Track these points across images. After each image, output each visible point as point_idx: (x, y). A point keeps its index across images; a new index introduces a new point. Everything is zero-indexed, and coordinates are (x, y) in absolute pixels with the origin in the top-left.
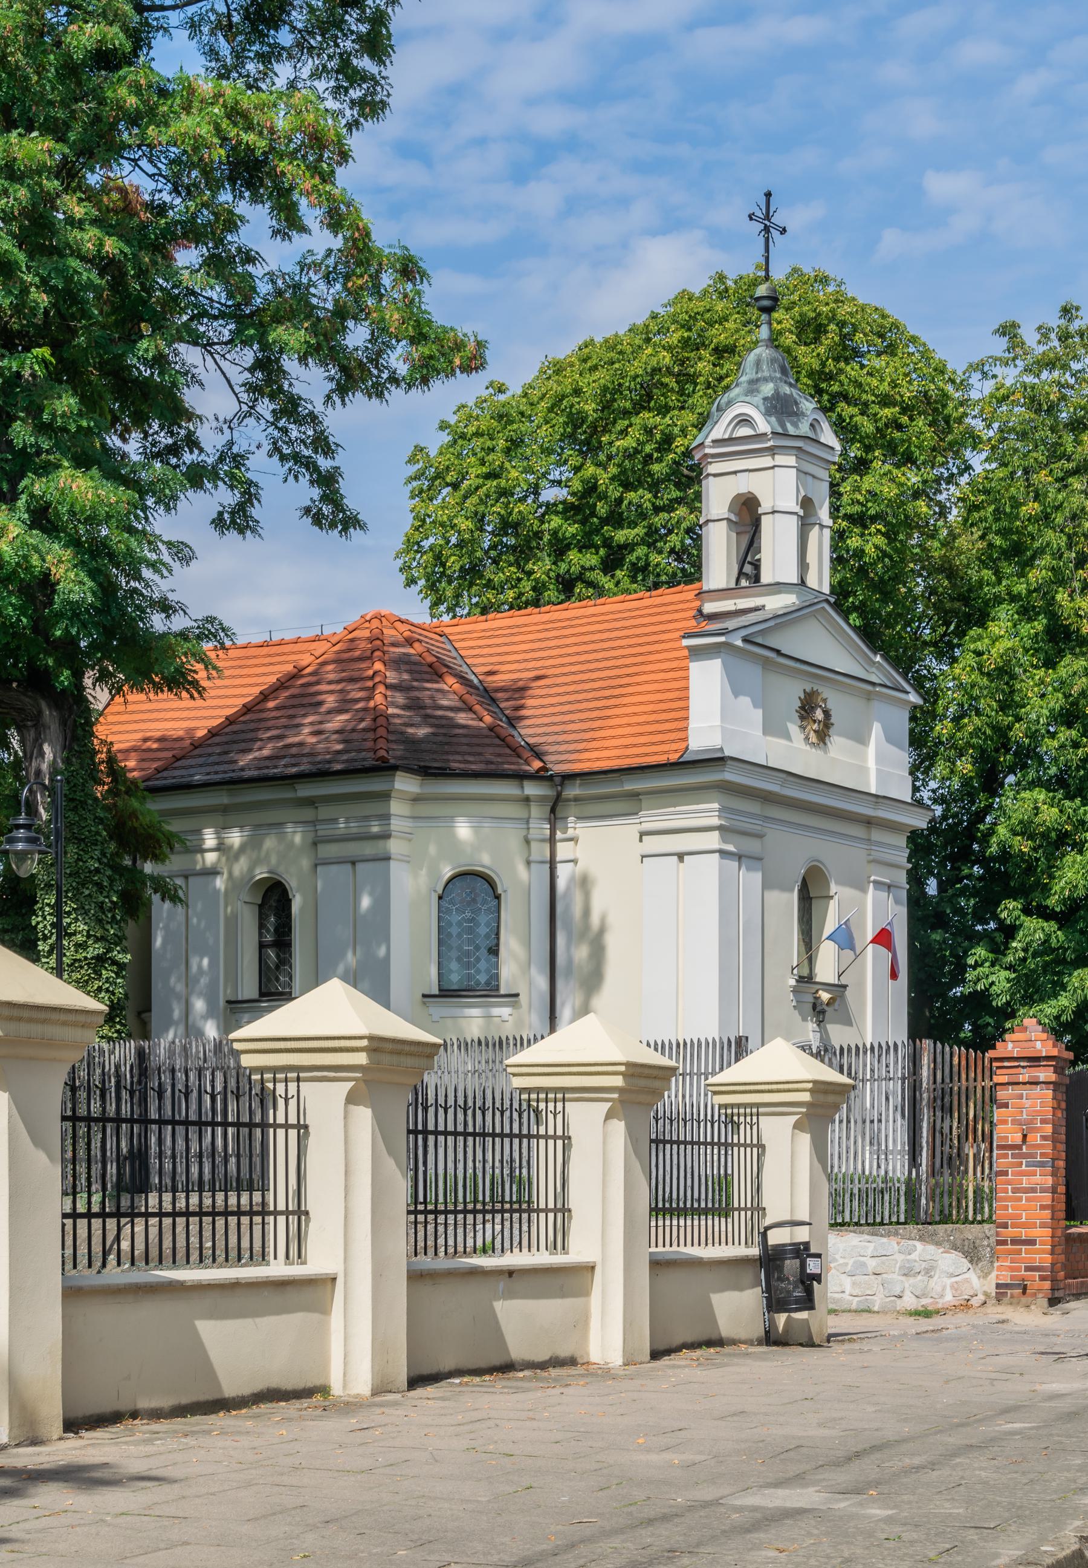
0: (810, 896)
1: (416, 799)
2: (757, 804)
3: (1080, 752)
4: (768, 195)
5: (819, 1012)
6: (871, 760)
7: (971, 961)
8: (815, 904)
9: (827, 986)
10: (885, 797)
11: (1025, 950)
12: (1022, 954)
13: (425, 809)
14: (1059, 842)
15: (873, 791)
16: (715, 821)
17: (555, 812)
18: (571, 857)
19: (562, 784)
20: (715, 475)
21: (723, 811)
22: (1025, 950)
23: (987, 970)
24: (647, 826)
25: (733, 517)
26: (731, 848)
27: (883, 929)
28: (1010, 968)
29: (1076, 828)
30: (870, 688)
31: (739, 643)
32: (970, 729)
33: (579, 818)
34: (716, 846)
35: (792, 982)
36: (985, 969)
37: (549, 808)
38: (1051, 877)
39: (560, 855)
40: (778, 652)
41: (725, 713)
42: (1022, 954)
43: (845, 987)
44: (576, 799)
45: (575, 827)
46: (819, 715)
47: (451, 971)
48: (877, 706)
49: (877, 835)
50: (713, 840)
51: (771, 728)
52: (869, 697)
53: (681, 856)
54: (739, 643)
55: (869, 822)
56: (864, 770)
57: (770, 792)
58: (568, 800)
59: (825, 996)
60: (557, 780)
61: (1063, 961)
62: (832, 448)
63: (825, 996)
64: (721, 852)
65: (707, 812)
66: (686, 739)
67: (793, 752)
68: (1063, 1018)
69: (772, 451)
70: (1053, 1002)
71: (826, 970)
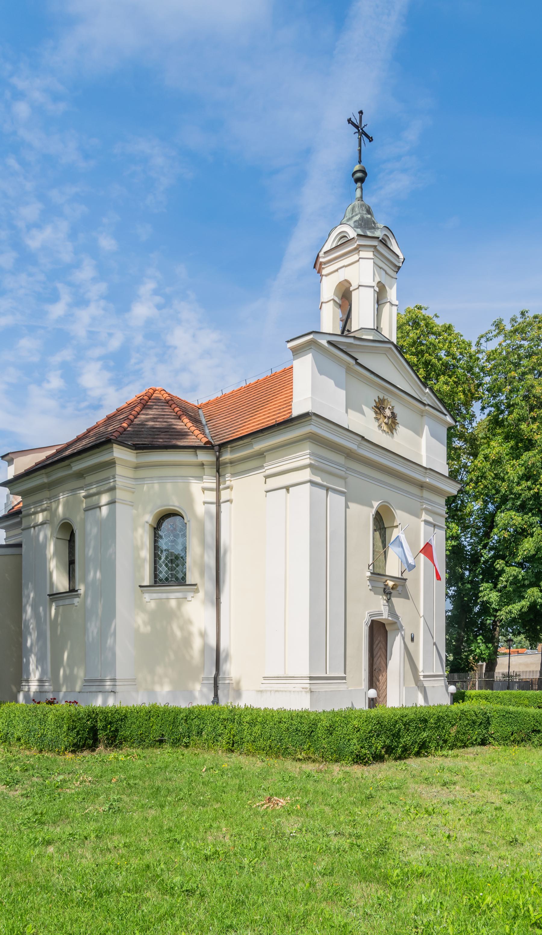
0: (381, 524)
1: (137, 467)
2: (343, 459)
3: (532, 492)
4: (361, 112)
5: (387, 593)
6: (424, 446)
7: (481, 589)
8: (388, 531)
9: (392, 578)
10: (430, 469)
11: (507, 581)
12: (505, 583)
13: (142, 473)
14: (522, 533)
15: (424, 465)
16: (308, 461)
17: (219, 469)
18: (228, 498)
19: (220, 449)
20: (326, 276)
21: (312, 454)
22: (507, 581)
23: (488, 592)
24: (268, 472)
25: (337, 299)
26: (318, 480)
27: (428, 543)
28: (499, 591)
29: (529, 526)
30: (421, 406)
31: (324, 342)
32: (482, 486)
33: (234, 475)
34: (308, 478)
35: (369, 574)
36: (487, 592)
37: (215, 470)
38: (517, 549)
39: (223, 498)
40: (356, 360)
41: (314, 388)
42: (505, 583)
43: (406, 580)
44: (232, 462)
45: (229, 480)
46: (388, 413)
47: (161, 572)
48: (426, 419)
49: (426, 494)
50: (306, 475)
51: (350, 405)
52: (422, 414)
53: (287, 488)
54: (324, 342)
55: (422, 486)
56: (420, 456)
57: (350, 450)
58: (226, 463)
59: (390, 583)
60: (217, 448)
61: (524, 586)
62: (398, 256)
63: (390, 583)
64: (312, 483)
65: (303, 456)
66: (291, 412)
67: (365, 423)
68: (523, 610)
69: (357, 250)
70: (519, 604)
71: (393, 568)
